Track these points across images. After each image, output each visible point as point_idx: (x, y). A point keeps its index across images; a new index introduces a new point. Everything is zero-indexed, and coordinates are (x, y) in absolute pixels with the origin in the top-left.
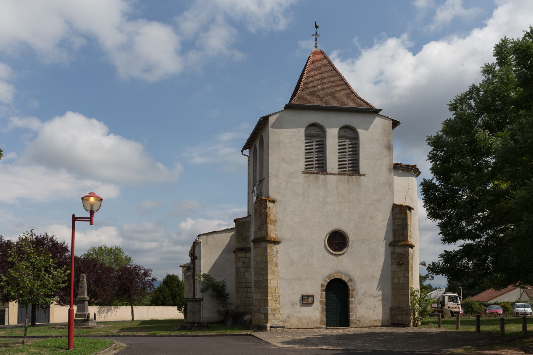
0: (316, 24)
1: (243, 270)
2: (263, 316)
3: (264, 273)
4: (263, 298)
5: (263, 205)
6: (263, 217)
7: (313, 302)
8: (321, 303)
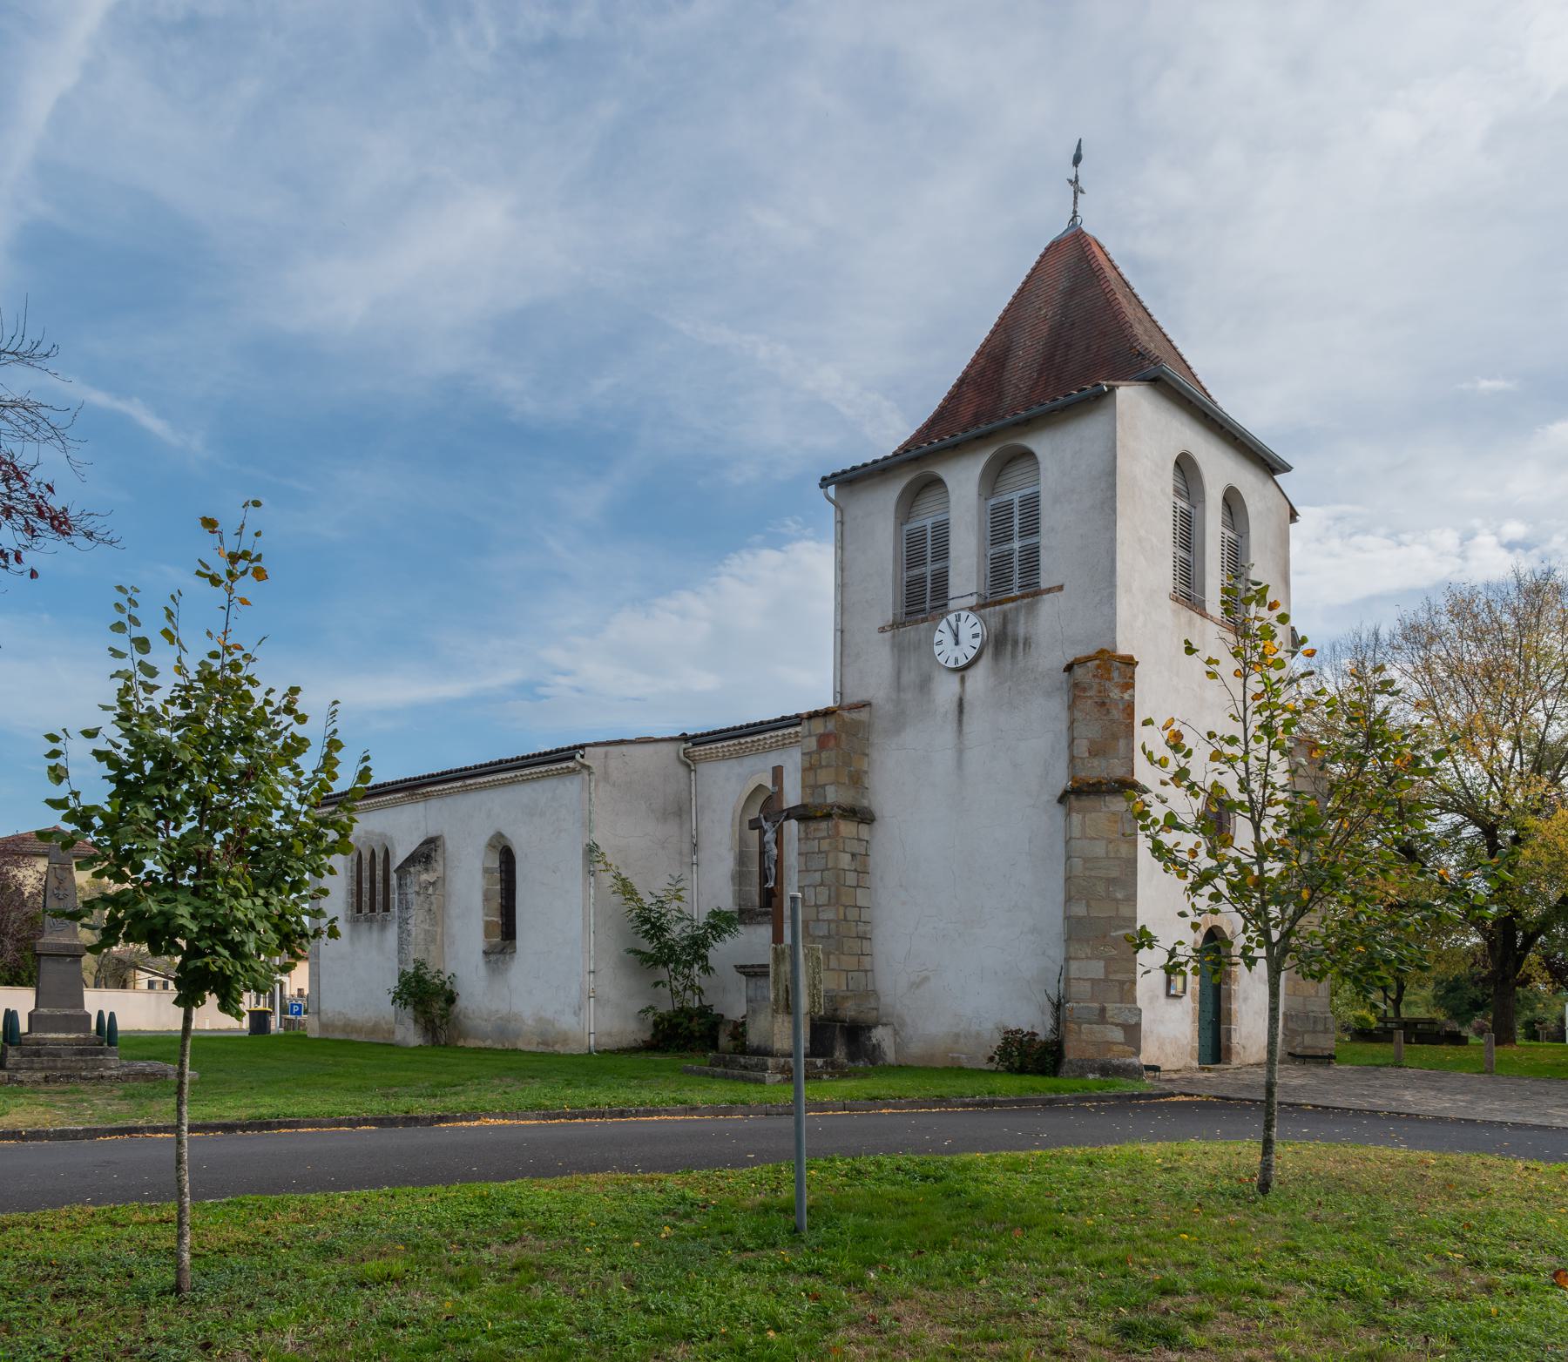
1: (851, 879)
2: (1118, 1035)
3: (1119, 896)
4: (1111, 977)
5: (1115, 674)
6: (1116, 714)
7: (1184, 991)
8: (1193, 995)
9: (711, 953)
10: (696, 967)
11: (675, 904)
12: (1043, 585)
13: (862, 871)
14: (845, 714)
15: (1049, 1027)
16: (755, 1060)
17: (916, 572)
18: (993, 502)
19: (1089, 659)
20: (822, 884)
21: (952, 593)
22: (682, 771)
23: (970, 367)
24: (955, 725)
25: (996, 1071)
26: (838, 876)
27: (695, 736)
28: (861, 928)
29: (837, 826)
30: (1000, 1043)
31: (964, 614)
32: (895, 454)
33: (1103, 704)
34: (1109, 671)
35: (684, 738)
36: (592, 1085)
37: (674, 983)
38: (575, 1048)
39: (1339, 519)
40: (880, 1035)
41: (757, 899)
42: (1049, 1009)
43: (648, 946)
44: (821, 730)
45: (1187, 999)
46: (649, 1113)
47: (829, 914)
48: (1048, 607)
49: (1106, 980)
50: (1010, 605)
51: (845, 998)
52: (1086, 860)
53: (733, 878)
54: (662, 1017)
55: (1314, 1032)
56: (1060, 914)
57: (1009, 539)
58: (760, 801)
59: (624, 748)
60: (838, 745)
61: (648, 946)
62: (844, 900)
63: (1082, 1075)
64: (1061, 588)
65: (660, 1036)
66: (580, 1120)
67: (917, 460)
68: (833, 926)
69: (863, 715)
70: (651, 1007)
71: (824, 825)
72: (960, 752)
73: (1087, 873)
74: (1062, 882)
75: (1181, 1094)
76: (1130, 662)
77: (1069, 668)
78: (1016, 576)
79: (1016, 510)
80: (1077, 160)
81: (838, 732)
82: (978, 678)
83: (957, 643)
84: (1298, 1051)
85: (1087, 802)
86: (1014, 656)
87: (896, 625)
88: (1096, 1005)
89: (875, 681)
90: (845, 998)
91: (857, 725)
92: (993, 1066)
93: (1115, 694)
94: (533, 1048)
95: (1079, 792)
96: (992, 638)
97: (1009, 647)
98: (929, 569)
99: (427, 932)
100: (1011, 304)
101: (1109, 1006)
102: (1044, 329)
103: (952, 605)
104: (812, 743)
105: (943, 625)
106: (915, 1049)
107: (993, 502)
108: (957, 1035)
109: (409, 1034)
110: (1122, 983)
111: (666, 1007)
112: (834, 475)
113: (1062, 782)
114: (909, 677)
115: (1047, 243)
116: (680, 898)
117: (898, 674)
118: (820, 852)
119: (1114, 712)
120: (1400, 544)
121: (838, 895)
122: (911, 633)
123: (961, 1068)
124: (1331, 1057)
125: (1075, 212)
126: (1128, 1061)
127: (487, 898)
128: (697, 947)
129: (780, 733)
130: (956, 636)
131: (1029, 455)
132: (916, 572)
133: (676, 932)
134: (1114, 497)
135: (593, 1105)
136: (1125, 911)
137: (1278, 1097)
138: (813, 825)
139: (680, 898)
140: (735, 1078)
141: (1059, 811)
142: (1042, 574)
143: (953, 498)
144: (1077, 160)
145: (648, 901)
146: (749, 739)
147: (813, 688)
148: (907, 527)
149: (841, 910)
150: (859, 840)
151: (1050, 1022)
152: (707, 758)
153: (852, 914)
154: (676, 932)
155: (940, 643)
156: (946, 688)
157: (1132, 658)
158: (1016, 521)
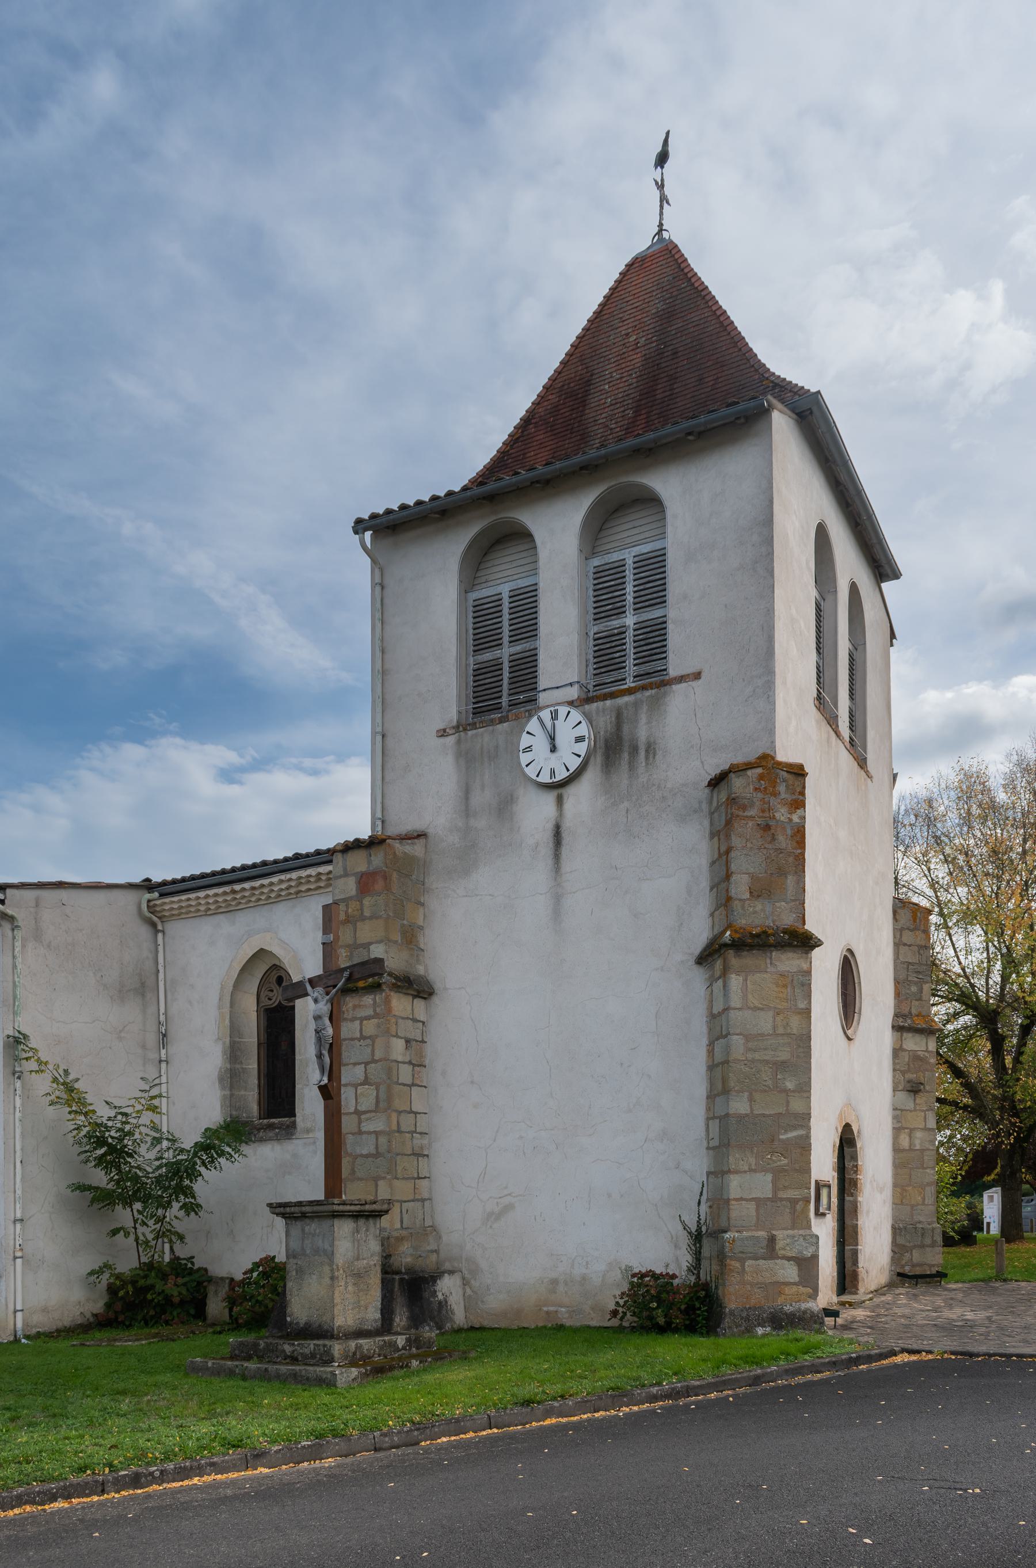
0: (666, 142)
2: (790, 1272)
3: (790, 1085)
4: (782, 1194)
5: (782, 788)
6: (783, 841)
9: (198, 1187)
10: (176, 1205)
11: (147, 1118)
12: (673, 672)
13: (418, 1064)
14: (397, 845)
15: (685, 1265)
16: (311, 1345)
17: (487, 656)
18: (596, 562)
19: (749, 766)
20: (366, 1082)
21: (543, 682)
22: (145, 931)
23: (536, 404)
24: (550, 862)
25: (620, 1329)
26: (389, 1071)
27: (164, 883)
28: (418, 1141)
29: (387, 1001)
30: (625, 1287)
31: (563, 710)
32: (465, 489)
33: (768, 827)
34: (774, 784)
35: (148, 885)
36: (55, 1416)
37: (141, 1229)
40: (448, 1288)
41: (255, 1108)
42: (684, 1240)
43: (100, 1178)
44: (363, 867)
45: (829, 1217)
46: (183, 1473)
47: (377, 1124)
48: (679, 701)
49: (775, 1199)
50: (626, 699)
51: (400, 1239)
52: (748, 1038)
53: (221, 1080)
54: (118, 1277)
55: (922, 1246)
56: (699, 1112)
57: (620, 612)
59: (63, 894)
60: (388, 888)
61: (100, 1178)
62: (398, 1104)
63: (749, 1331)
64: (697, 676)
65: (119, 1306)
66: (60, 1504)
67: (492, 499)
68: (383, 1140)
69: (416, 849)
70: (107, 1266)
71: (368, 1000)
72: (557, 899)
73: (750, 1056)
74: (703, 1069)
75: (903, 1350)
76: (798, 772)
77: (717, 781)
78: (630, 661)
79: (630, 576)
80: (662, 159)
81: (381, 869)
82: (582, 798)
83: (553, 749)
84: (907, 1269)
85: (749, 959)
86: (632, 767)
87: (461, 727)
88: (762, 1234)
89: (433, 798)
90: (400, 1239)
91: (411, 860)
92: (615, 1322)
93: (782, 814)
95: (730, 948)
96: (601, 743)
97: (626, 756)
98: (506, 652)
99: (181, 1208)
100: (586, 330)
101: (780, 1234)
102: (637, 360)
103: (543, 698)
104: (349, 886)
105: (533, 725)
106: (494, 1304)
107: (596, 562)
108: (555, 1282)
110: (794, 1202)
111: (127, 1263)
112: (374, 516)
113: (700, 932)
114: (483, 797)
115: (628, 259)
116: (154, 1109)
118: (363, 1037)
119: (781, 838)
121: (389, 1099)
122: (484, 737)
123: (561, 1328)
124: (941, 1275)
125: (661, 225)
126: (804, 1306)
128: (179, 1178)
129: (294, 875)
130: (552, 738)
131: (652, 502)
132: (487, 656)
133: (146, 1158)
134: (770, 554)
135: (82, 1469)
136: (796, 1106)
139: (154, 1109)
140: (283, 1379)
141: (698, 977)
142: (671, 656)
143: (543, 553)
144: (662, 159)
145: (104, 1113)
146: (247, 885)
147: (341, 808)
148: (474, 595)
149: (394, 1116)
150: (415, 1020)
151: (686, 1259)
152: (180, 915)
153: (407, 1122)
154: (146, 1158)
155: (528, 749)
156: (536, 813)
157: (801, 767)
158: (630, 588)
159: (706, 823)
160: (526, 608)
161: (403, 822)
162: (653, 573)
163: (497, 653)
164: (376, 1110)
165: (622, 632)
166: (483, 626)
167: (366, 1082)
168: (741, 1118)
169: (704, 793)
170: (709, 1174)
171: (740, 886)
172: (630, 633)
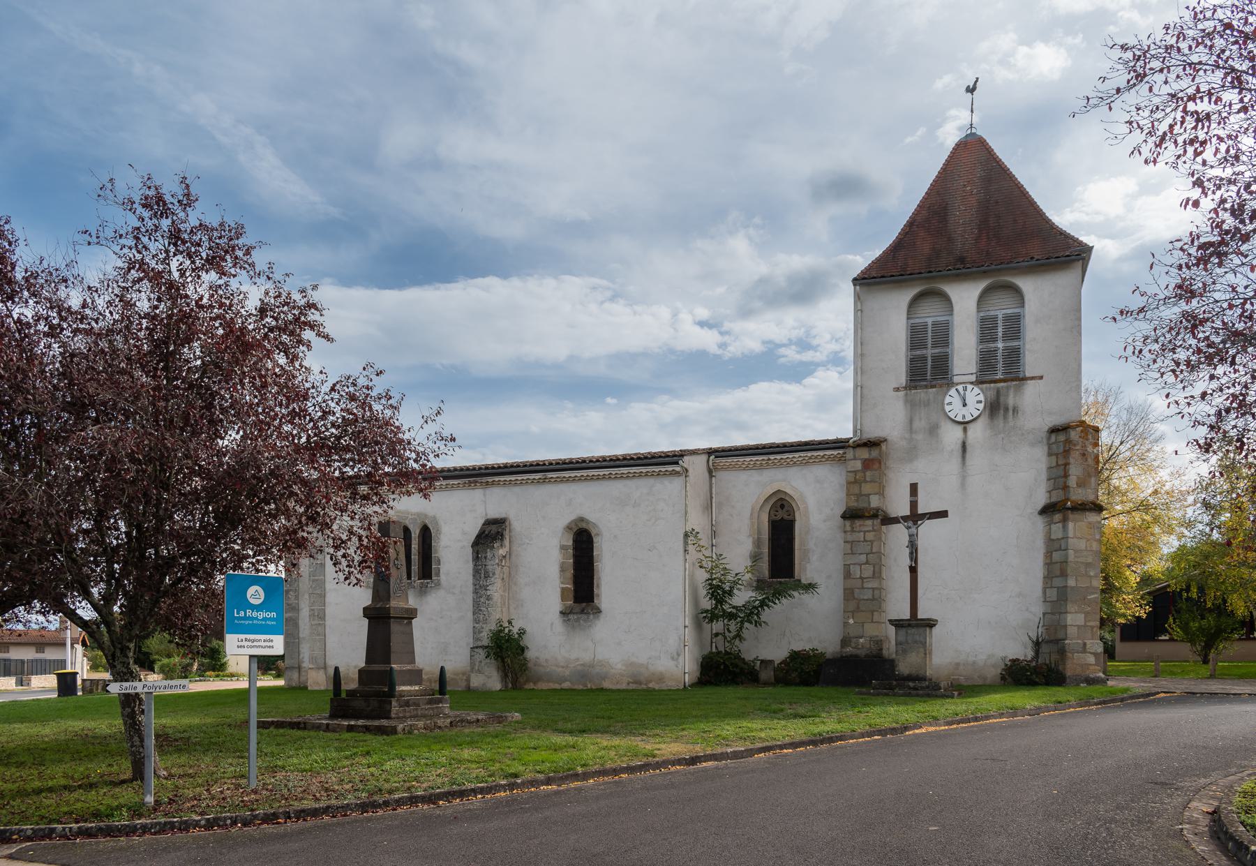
17: (918, 352)
20: (867, 563)
24: (960, 459)
35: (710, 452)
38: (672, 685)
39: (594, 288)
41: (767, 573)
42: (1030, 644)
48: (1030, 388)
49: (1085, 626)
52: (1076, 551)
57: (995, 340)
58: (774, 499)
64: (1041, 378)
71: (869, 522)
72: (963, 478)
77: (1054, 430)
79: (1000, 323)
80: (971, 90)
81: (864, 454)
83: (965, 405)
85: (1076, 516)
86: (1005, 418)
89: (891, 420)
93: (1090, 449)
94: (624, 686)
101: (1088, 642)
104: (858, 465)
105: (953, 392)
108: (958, 664)
109: (490, 679)
113: (1041, 499)
117: (911, 421)
118: (865, 541)
120: (635, 313)
122: (921, 394)
127: (563, 569)
129: (809, 454)
132: (918, 352)
134: (1080, 325)
137: (152, 722)
138: (858, 523)
141: (1040, 522)
151: (1030, 654)
155: (950, 404)
156: (952, 435)
158: (1000, 329)
159: (1046, 448)
160: (943, 335)
161: (872, 433)
162: (1014, 327)
163: (924, 352)
164: (874, 577)
165: (996, 350)
166: (916, 338)
167: (867, 563)
168: (1072, 588)
169: (1044, 435)
170: (1044, 614)
171: (1072, 482)
172: (1000, 353)
